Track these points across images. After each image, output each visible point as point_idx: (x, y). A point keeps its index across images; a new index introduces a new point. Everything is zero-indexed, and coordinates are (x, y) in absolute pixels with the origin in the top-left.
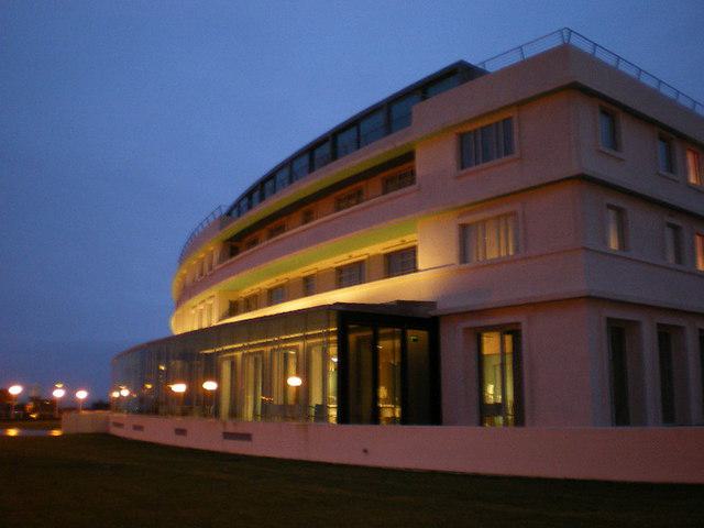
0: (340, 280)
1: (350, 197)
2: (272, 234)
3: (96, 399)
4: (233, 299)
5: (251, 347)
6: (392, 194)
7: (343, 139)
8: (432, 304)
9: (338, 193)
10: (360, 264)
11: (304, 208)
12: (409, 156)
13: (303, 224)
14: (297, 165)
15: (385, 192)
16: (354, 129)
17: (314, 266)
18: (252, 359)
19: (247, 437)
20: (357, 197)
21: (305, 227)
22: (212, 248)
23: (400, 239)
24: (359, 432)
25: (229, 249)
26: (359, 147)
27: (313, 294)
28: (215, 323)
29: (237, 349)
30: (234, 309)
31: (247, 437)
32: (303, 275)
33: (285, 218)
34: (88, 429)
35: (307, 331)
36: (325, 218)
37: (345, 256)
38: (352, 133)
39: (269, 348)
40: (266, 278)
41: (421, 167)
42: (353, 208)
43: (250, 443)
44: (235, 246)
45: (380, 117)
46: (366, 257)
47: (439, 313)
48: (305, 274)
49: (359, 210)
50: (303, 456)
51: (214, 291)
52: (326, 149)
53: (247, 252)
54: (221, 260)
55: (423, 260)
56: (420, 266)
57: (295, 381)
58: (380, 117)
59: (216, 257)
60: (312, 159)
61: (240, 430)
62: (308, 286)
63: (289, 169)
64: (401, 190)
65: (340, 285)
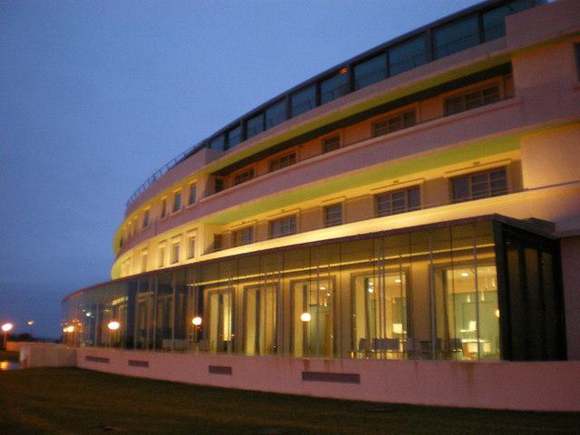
0: (379, 207)
1: (245, 175)
2: (239, 180)
3: (19, 332)
4: (218, 233)
5: (270, 277)
6: (276, 172)
7: (251, 124)
8: (550, 225)
9: (326, 135)
10: (250, 229)
11: (329, 136)
12: (504, 70)
13: (373, 137)
14: (233, 135)
15: (271, 170)
16: (261, 117)
17: (341, 193)
18: (254, 292)
19: (354, 378)
20: (409, 120)
21: (270, 174)
22: (197, 179)
23: (394, 180)
24: (224, 356)
25: (214, 185)
26: (265, 130)
27: (296, 233)
28: (199, 257)
29: (72, 297)
30: (218, 243)
31: (354, 378)
32: (322, 205)
33: (297, 147)
34: (56, 363)
35: (320, 264)
36: (314, 158)
37: (390, 182)
38: (259, 120)
39: (287, 280)
40: (269, 209)
41: (522, 77)
42: (316, 159)
43: (208, 373)
44: (219, 181)
45: (283, 106)
46: (421, 181)
47: (559, 236)
48: (325, 204)
49: (283, 173)
50: (463, 402)
51: (200, 224)
52: (238, 131)
53: (279, 171)
54: (207, 193)
55: (528, 180)
56: (526, 184)
57: (197, 321)
58: (283, 106)
59: (200, 190)
60: (319, 92)
61: (347, 370)
62: (332, 215)
63: (288, 103)
64: (469, 112)
65: (271, 236)
